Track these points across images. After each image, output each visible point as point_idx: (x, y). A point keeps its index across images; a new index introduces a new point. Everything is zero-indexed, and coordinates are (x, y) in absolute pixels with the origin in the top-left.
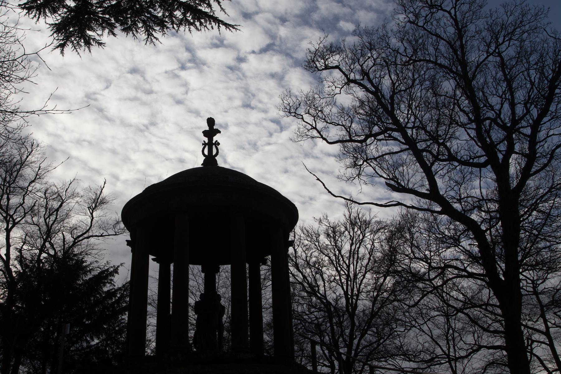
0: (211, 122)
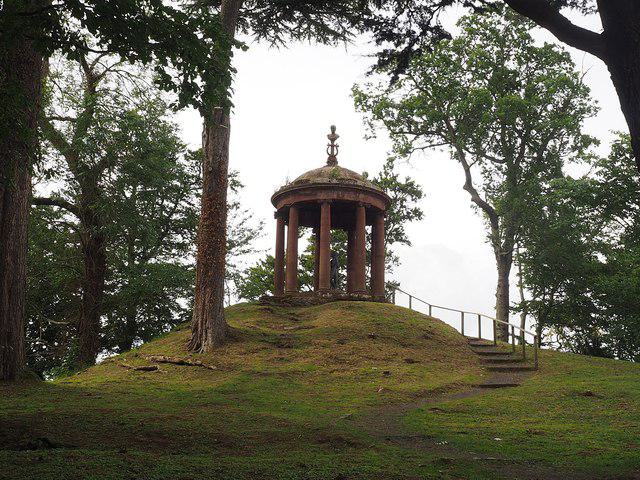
0: (333, 129)
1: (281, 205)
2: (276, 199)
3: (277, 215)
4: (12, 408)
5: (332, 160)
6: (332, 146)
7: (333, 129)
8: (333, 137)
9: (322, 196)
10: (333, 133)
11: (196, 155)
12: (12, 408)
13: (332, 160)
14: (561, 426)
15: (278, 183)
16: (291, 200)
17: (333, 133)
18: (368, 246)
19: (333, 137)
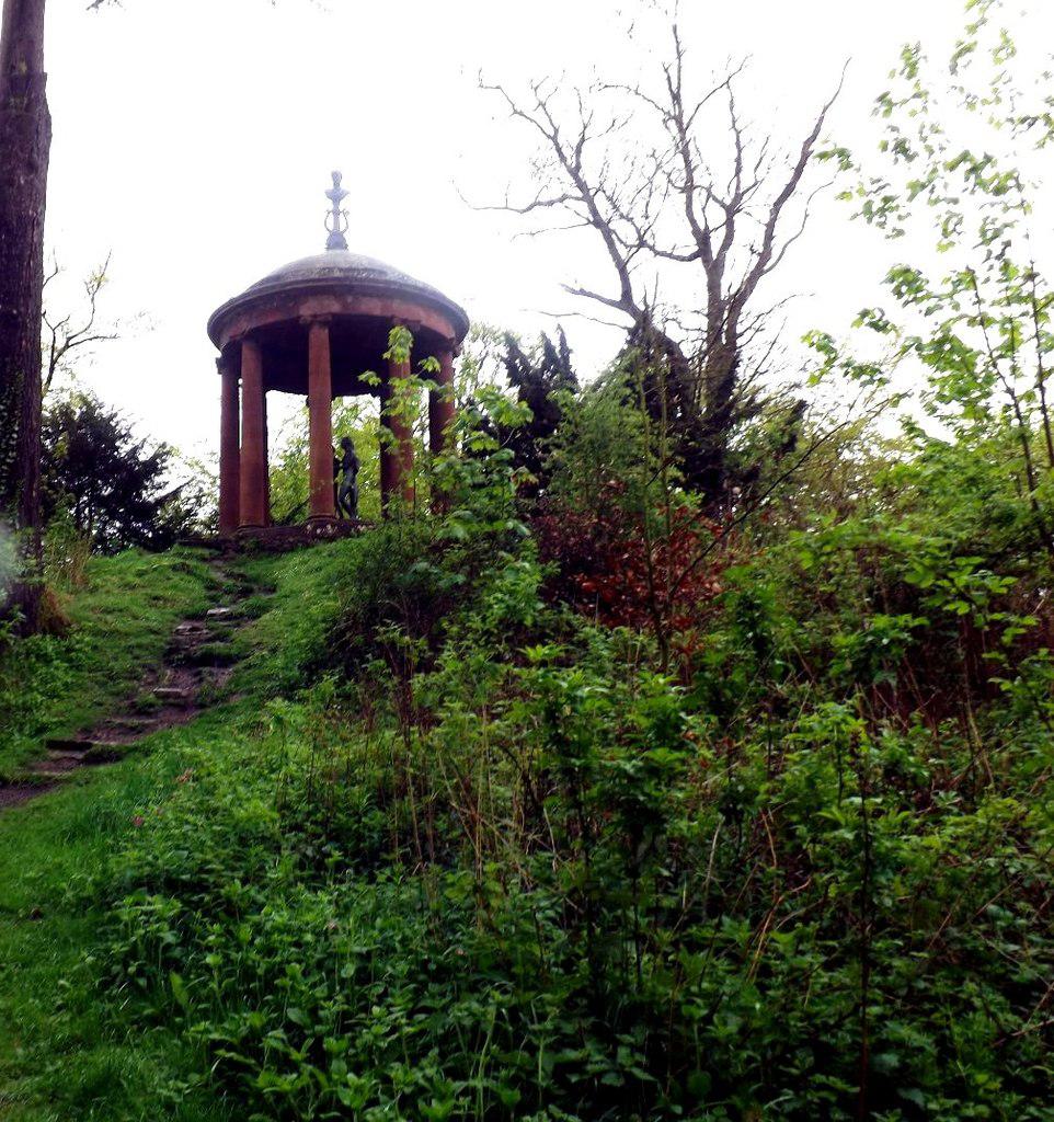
0: (336, 177)
1: (225, 341)
2: (219, 327)
3: (222, 365)
4: (387, 1035)
5: (337, 241)
6: (336, 213)
7: (336, 177)
8: (336, 196)
9: (306, 310)
10: (336, 184)
11: (964, 416)
12: (387, 1035)
13: (337, 241)
14: (54, 774)
15: (237, 284)
16: (245, 325)
17: (336, 184)
18: (240, 381)
19: (336, 196)
